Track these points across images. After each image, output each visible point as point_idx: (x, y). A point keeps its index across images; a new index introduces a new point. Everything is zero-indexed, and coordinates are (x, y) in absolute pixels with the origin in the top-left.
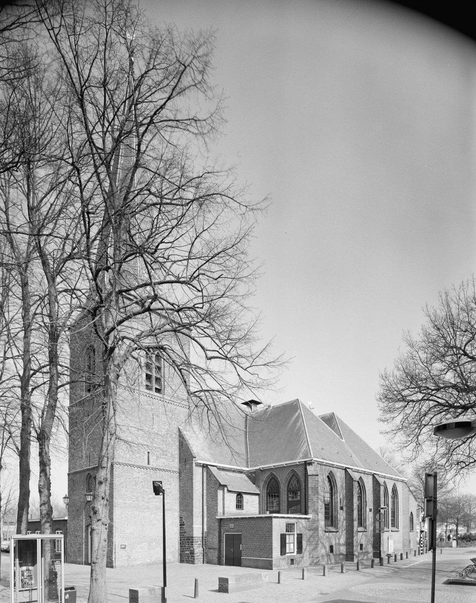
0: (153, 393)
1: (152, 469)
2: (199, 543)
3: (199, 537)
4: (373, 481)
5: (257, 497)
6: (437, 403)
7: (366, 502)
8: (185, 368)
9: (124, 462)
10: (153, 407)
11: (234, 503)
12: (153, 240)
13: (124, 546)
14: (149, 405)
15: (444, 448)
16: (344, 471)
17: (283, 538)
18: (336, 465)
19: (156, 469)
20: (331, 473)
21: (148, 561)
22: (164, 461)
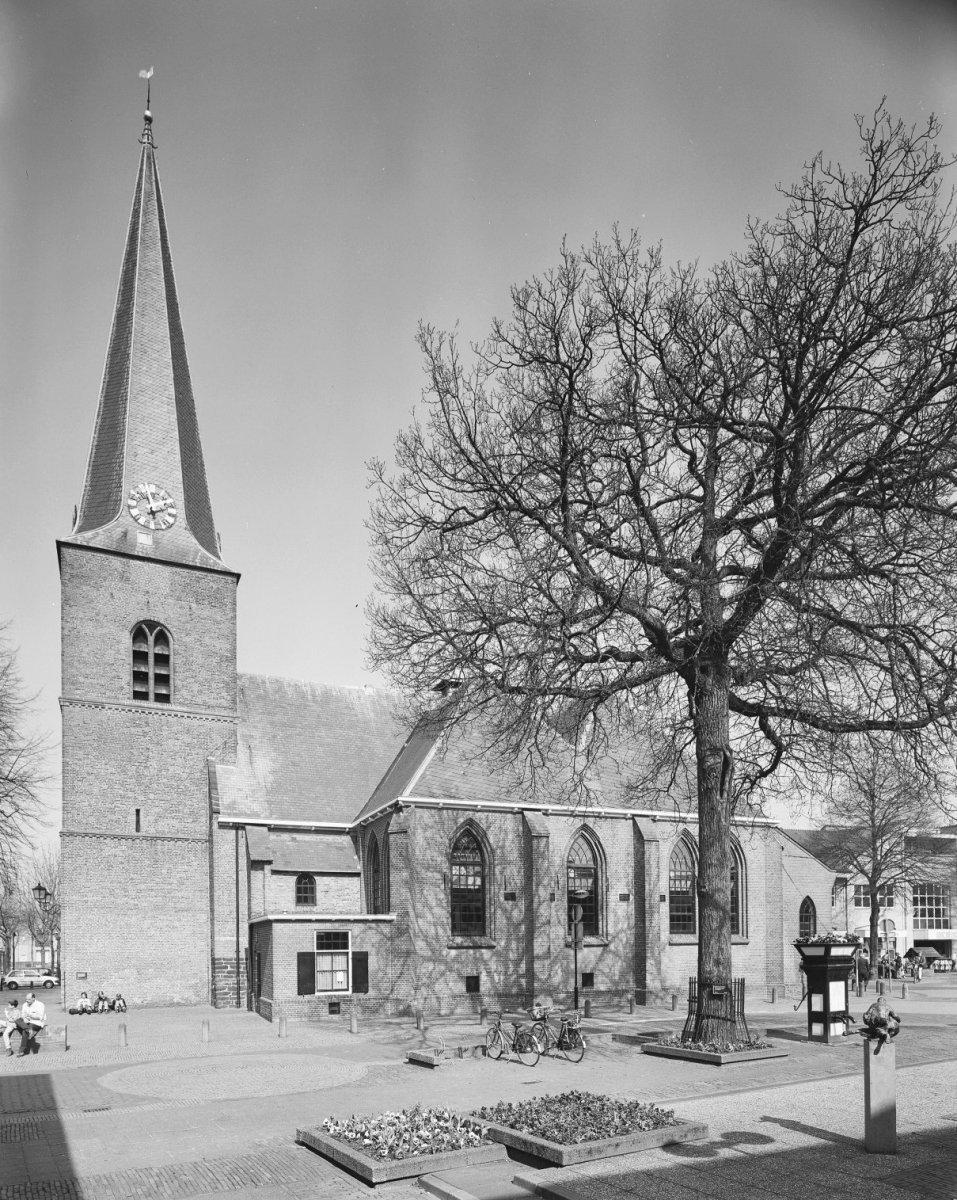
0: (151, 704)
1: (145, 838)
2: (229, 969)
3: (231, 960)
4: (635, 833)
5: (356, 879)
6: (802, 949)
7: (607, 880)
8: (879, 853)
9: (81, 831)
10: (146, 729)
11: (292, 894)
12: (611, 711)
13: (83, 975)
14: (139, 726)
15: (843, 679)
16: (631, 821)
17: (306, 963)
18: (444, 804)
19: (154, 839)
20: (585, 827)
21: (139, 1002)
22: (175, 822)
